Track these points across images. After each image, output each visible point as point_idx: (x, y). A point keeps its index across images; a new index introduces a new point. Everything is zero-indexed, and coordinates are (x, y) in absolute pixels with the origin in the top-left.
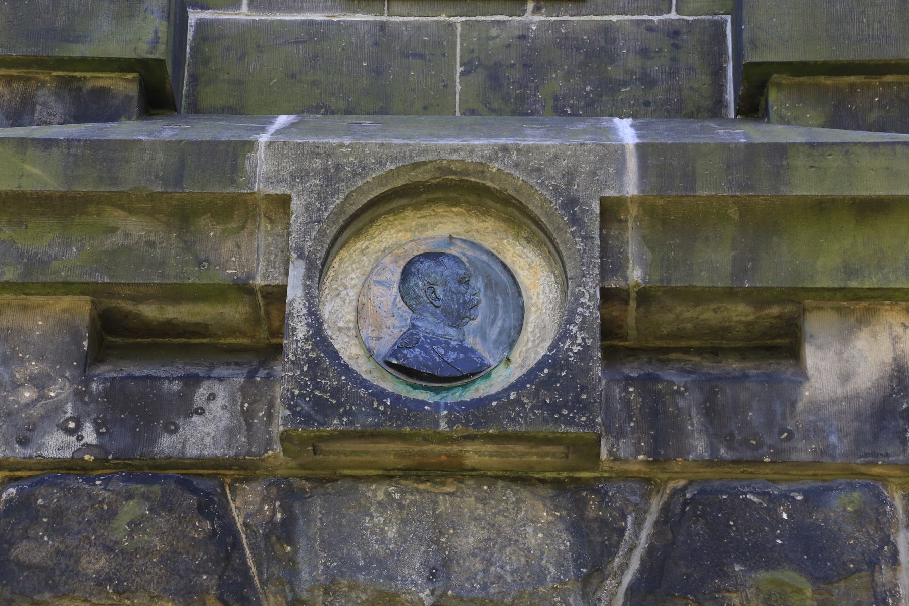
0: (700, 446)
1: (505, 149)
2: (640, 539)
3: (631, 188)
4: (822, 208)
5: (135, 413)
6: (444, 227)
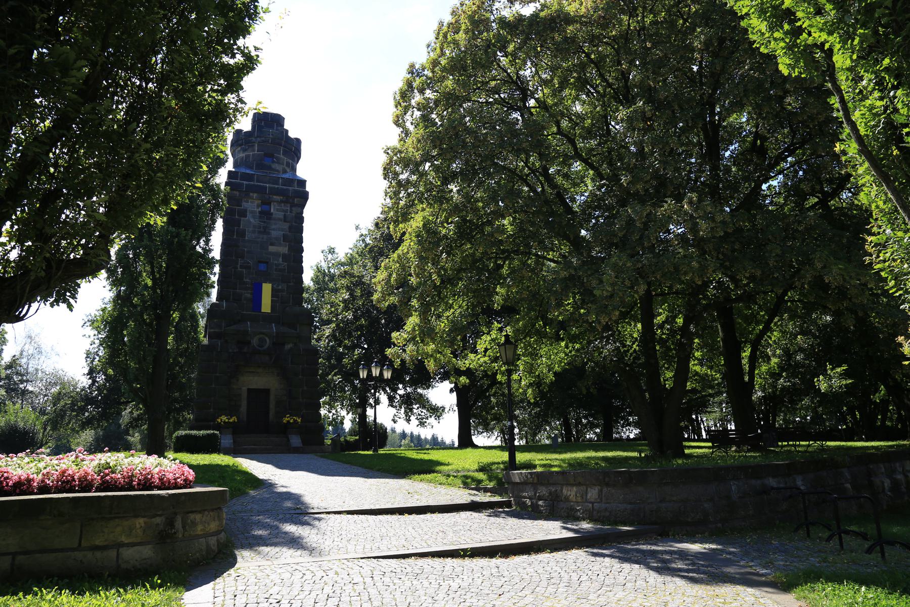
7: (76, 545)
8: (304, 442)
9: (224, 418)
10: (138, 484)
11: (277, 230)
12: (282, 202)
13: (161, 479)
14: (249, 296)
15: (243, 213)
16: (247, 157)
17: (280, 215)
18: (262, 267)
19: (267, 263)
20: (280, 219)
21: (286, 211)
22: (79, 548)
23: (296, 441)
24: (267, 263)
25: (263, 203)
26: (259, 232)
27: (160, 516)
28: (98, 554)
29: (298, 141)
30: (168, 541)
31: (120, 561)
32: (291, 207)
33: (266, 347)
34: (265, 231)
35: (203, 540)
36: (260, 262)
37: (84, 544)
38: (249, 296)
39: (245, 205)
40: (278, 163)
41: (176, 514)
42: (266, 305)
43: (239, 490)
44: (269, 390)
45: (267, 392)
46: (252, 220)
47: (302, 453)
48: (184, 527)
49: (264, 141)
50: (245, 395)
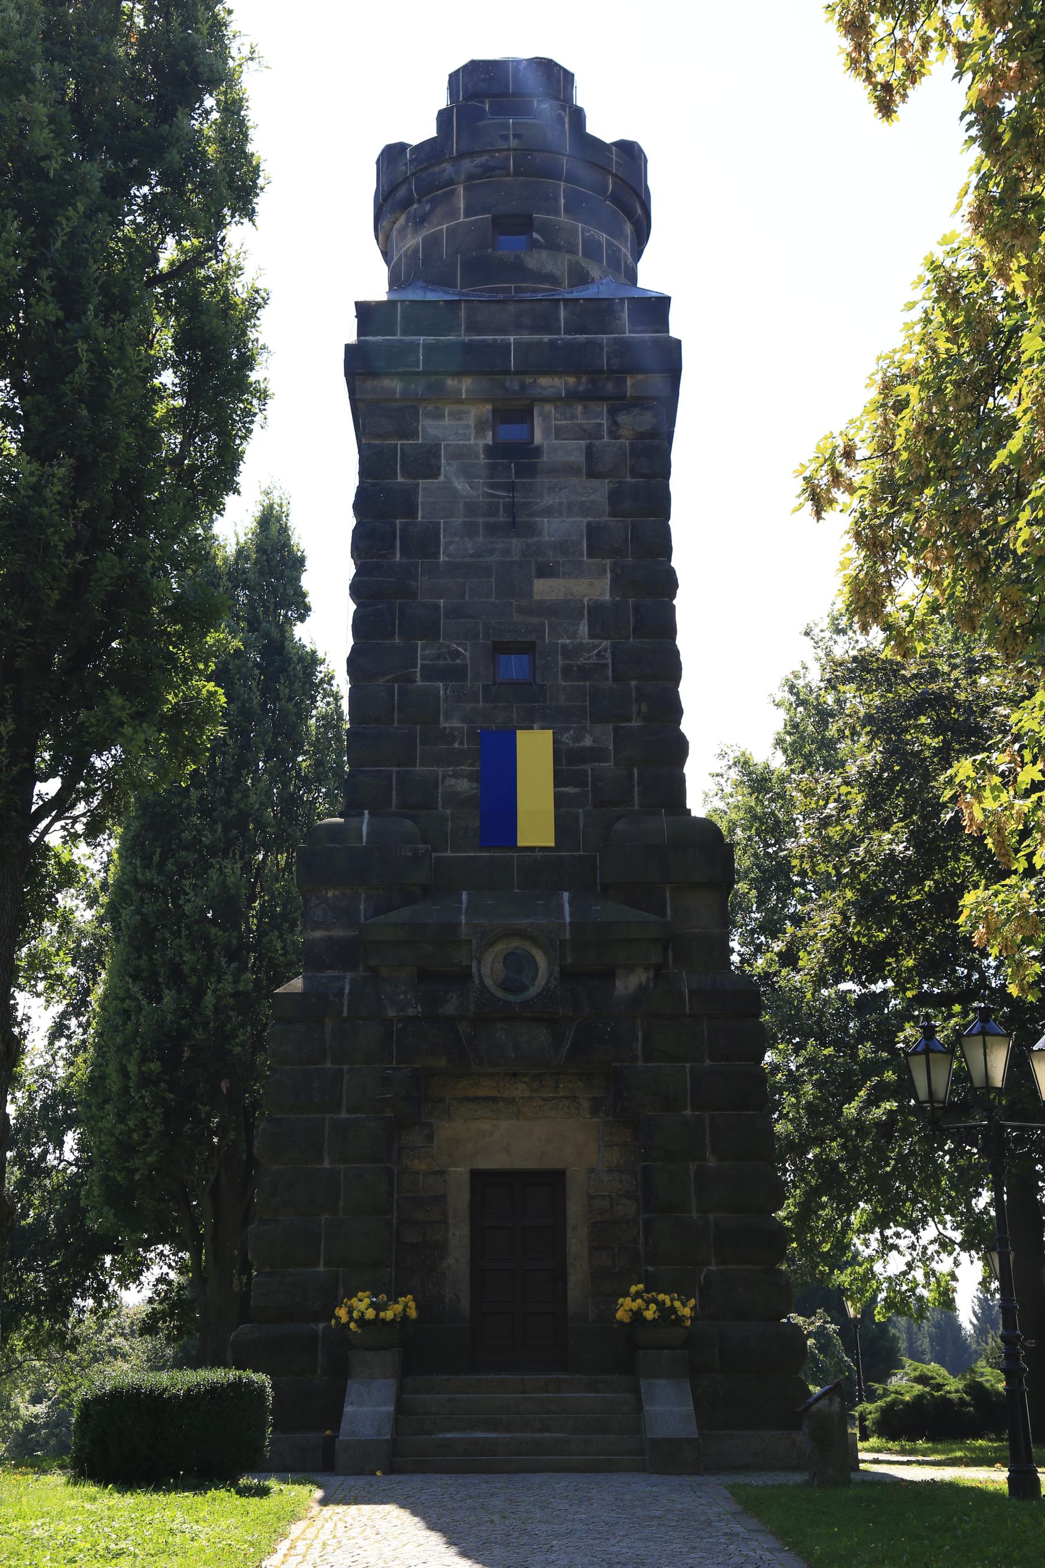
1: (532, 924)
3: (568, 937)
6: (515, 943)
11: (564, 511)
12: (573, 396)
14: (463, 786)
15: (426, 462)
16: (431, 243)
17: (573, 451)
20: (570, 470)
21: (595, 434)
23: (669, 1409)
26: (492, 529)
29: (630, 154)
32: (613, 412)
33: (533, 991)
34: (515, 521)
39: (429, 428)
40: (552, 246)
42: (536, 822)
45: (552, 1181)
46: (460, 485)
49: (487, 170)
50: (460, 1198)
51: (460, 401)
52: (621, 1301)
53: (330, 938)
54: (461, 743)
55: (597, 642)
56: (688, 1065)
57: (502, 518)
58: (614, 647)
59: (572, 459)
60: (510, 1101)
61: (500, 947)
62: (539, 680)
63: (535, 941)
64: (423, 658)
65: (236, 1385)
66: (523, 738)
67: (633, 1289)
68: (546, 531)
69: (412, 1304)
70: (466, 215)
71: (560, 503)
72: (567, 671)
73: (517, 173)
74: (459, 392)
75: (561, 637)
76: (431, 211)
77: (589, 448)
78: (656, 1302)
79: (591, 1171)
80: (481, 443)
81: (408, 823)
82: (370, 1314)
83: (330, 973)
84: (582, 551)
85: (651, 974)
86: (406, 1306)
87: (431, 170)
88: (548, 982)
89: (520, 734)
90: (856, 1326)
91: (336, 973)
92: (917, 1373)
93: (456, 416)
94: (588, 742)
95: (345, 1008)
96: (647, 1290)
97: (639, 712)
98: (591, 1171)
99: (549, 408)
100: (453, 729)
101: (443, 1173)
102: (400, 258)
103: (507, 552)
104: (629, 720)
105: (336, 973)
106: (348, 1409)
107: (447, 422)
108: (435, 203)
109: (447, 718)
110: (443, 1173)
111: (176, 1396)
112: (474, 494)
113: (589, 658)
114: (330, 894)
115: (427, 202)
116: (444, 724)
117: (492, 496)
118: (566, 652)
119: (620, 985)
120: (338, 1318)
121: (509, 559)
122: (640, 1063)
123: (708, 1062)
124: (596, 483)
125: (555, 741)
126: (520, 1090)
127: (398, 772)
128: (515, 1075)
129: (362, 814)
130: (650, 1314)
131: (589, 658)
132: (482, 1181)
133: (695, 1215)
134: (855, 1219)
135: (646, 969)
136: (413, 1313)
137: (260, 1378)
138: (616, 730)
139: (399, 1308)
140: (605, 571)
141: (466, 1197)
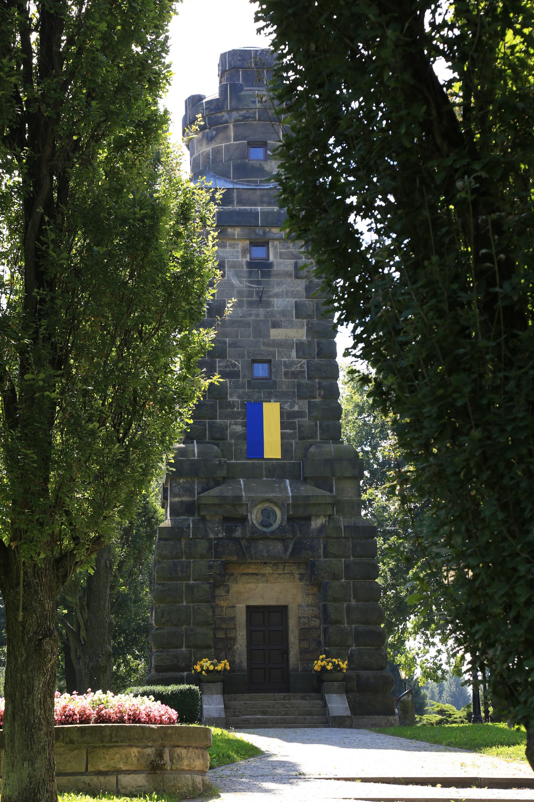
0: (299, 535)
2: (291, 546)
4: (313, 504)
5: (229, 531)
6: (267, 505)
7: (84, 770)
8: (353, 708)
9: (206, 664)
10: (129, 719)
13: (148, 715)
14: (239, 429)
16: (217, 151)
17: (288, 265)
18: (261, 370)
19: (269, 362)
20: (287, 274)
22: (86, 772)
23: (338, 705)
24: (269, 362)
25: (254, 244)
26: (251, 304)
27: (151, 747)
28: (102, 779)
30: (158, 772)
31: (119, 787)
33: (275, 526)
34: (261, 300)
35: (188, 776)
36: (254, 361)
37: (90, 769)
38: (239, 429)
41: (164, 746)
42: (272, 447)
43: (229, 757)
44: (285, 608)
45: (282, 611)
47: (351, 727)
48: (171, 760)
49: (245, 118)
50: (242, 618)
51: (235, 239)
52: (316, 662)
53: (182, 501)
54: (238, 408)
55: (300, 360)
56: (343, 560)
57: (255, 298)
58: (308, 363)
59: (288, 269)
60: (264, 575)
61: (260, 506)
62: (273, 378)
63: (276, 504)
64: (219, 367)
65: (190, 689)
66: (266, 406)
67: (321, 657)
68: (275, 305)
69: (228, 664)
70: (235, 140)
71: (282, 291)
72: (286, 374)
73: (260, 120)
74: (234, 235)
75: (283, 358)
76: (217, 134)
77: (296, 264)
78: (332, 662)
79: (300, 606)
80: (244, 260)
81: (215, 447)
82: (211, 668)
83: (182, 517)
84: (293, 315)
85: (327, 519)
86: (225, 664)
87: (217, 115)
88: (282, 523)
89: (265, 405)
90: (405, 684)
91: (185, 518)
92: (439, 709)
93: (232, 246)
94: (296, 408)
95: (191, 534)
96: (326, 658)
97: (320, 394)
98: (300, 606)
99: (277, 243)
100: (234, 401)
101: (234, 607)
102: (199, 155)
103: (258, 315)
104: (315, 397)
105: (185, 518)
106: (204, 706)
107: (228, 249)
108: (218, 131)
109: (231, 396)
110: (234, 607)
111: (168, 694)
112: (242, 286)
113: (297, 368)
114: (181, 481)
115: (214, 130)
116: (229, 399)
117: (250, 287)
118: (286, 365)
119: (313, 523)
120: (195, 670)
121: (259, 319)
122: (322, 559)
123: (352, 558)
124: (299, 281)
125: (281, 408)
126: (268, 570)
127: (209, 423)
128: (265, 563)
129: (193, 442)
130: (329, 667)
131: (297, 368)
132: (251, 610)
133: (346, 625)
134: (410, 625)
135: (325, 516)
136: (228, 668)
137: (193, 687)
138: (309, 403)
139: (223, 665)
140: (304, 325)
141: (244, 617)
